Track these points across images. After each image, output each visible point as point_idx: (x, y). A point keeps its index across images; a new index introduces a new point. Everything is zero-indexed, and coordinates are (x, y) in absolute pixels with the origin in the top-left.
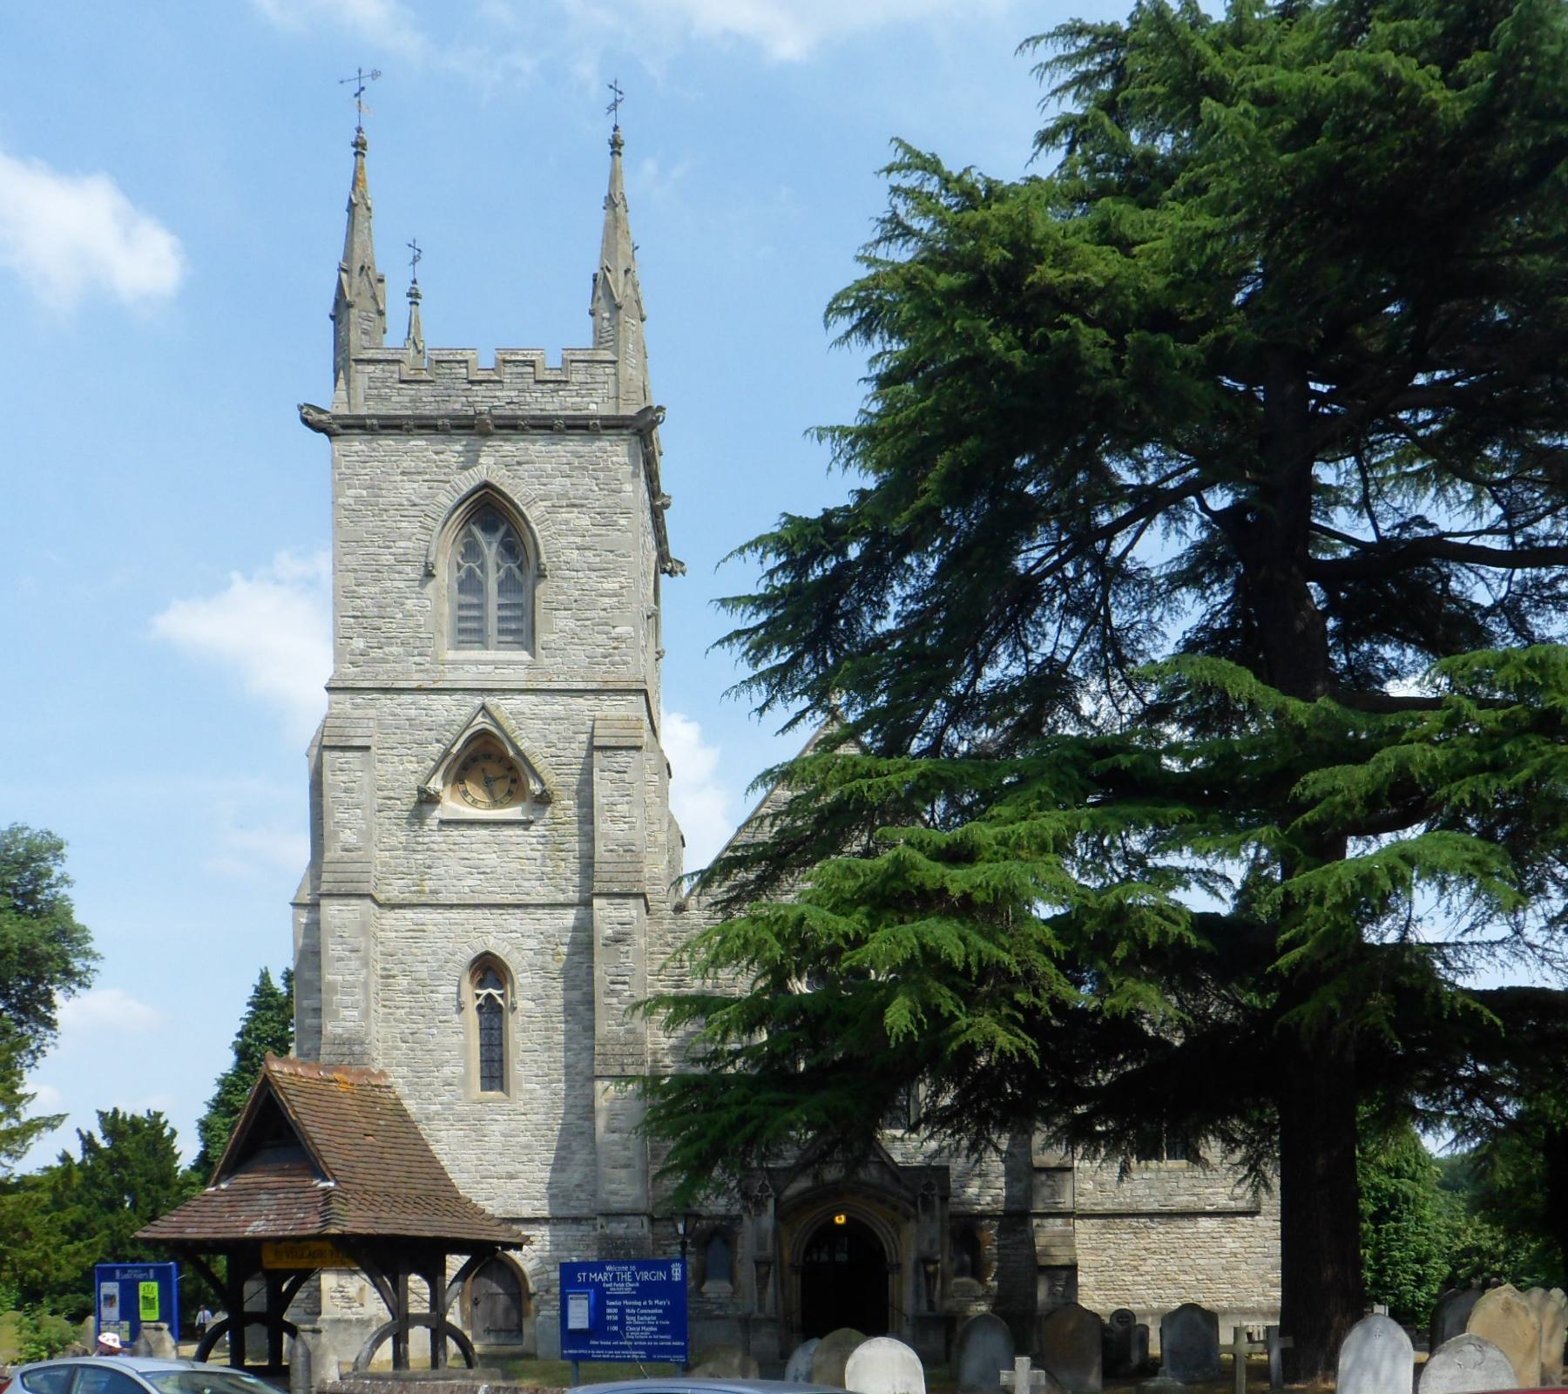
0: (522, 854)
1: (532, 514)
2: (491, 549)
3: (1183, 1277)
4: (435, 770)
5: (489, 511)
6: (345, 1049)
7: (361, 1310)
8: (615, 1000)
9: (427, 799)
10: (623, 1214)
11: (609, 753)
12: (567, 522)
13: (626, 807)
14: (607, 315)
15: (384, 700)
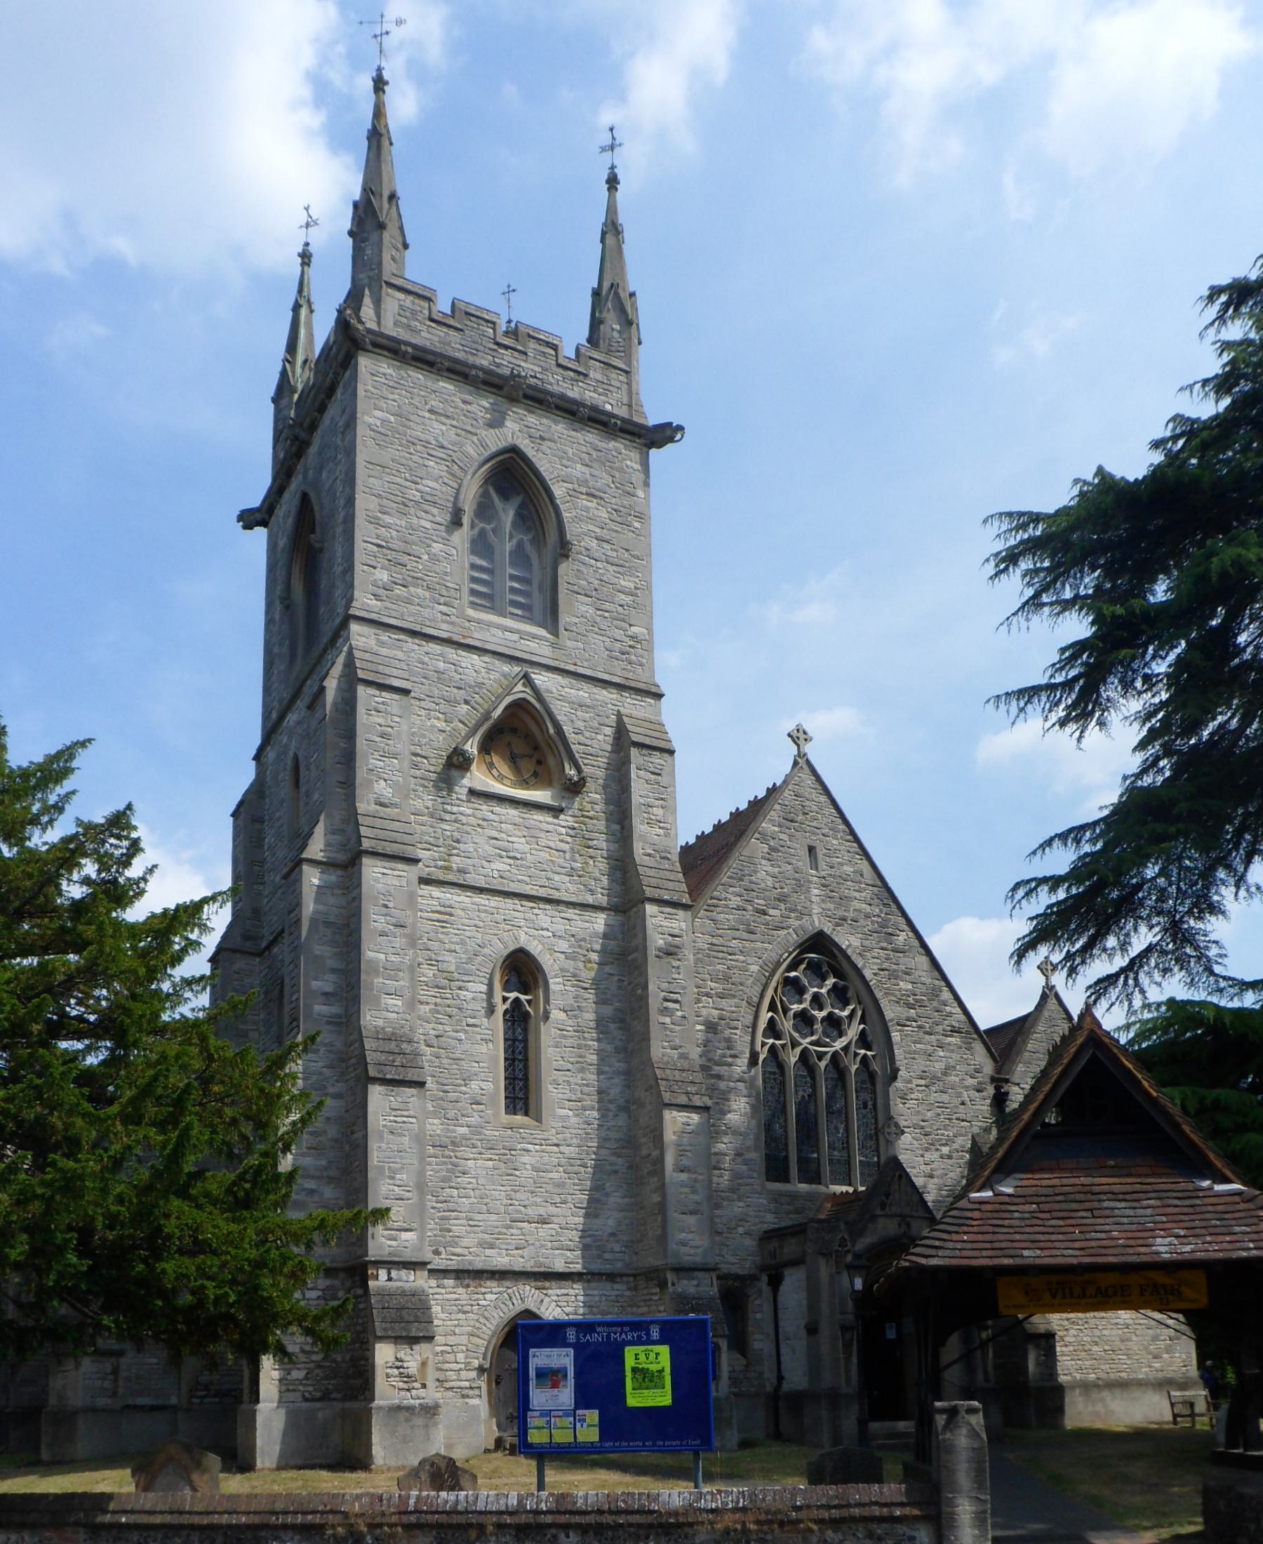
0: (552, 844)
1: (558, 491)
2: (507, 514)
3: (1095, 1348)
5: (512, 476)
6: (392, 1046)
7: (422, 1392)
8: (668, 1020)
9: (457, 762)
10: (694, 1270)
11: (644, 752)
12: (587, 509)
14: (618, 327)
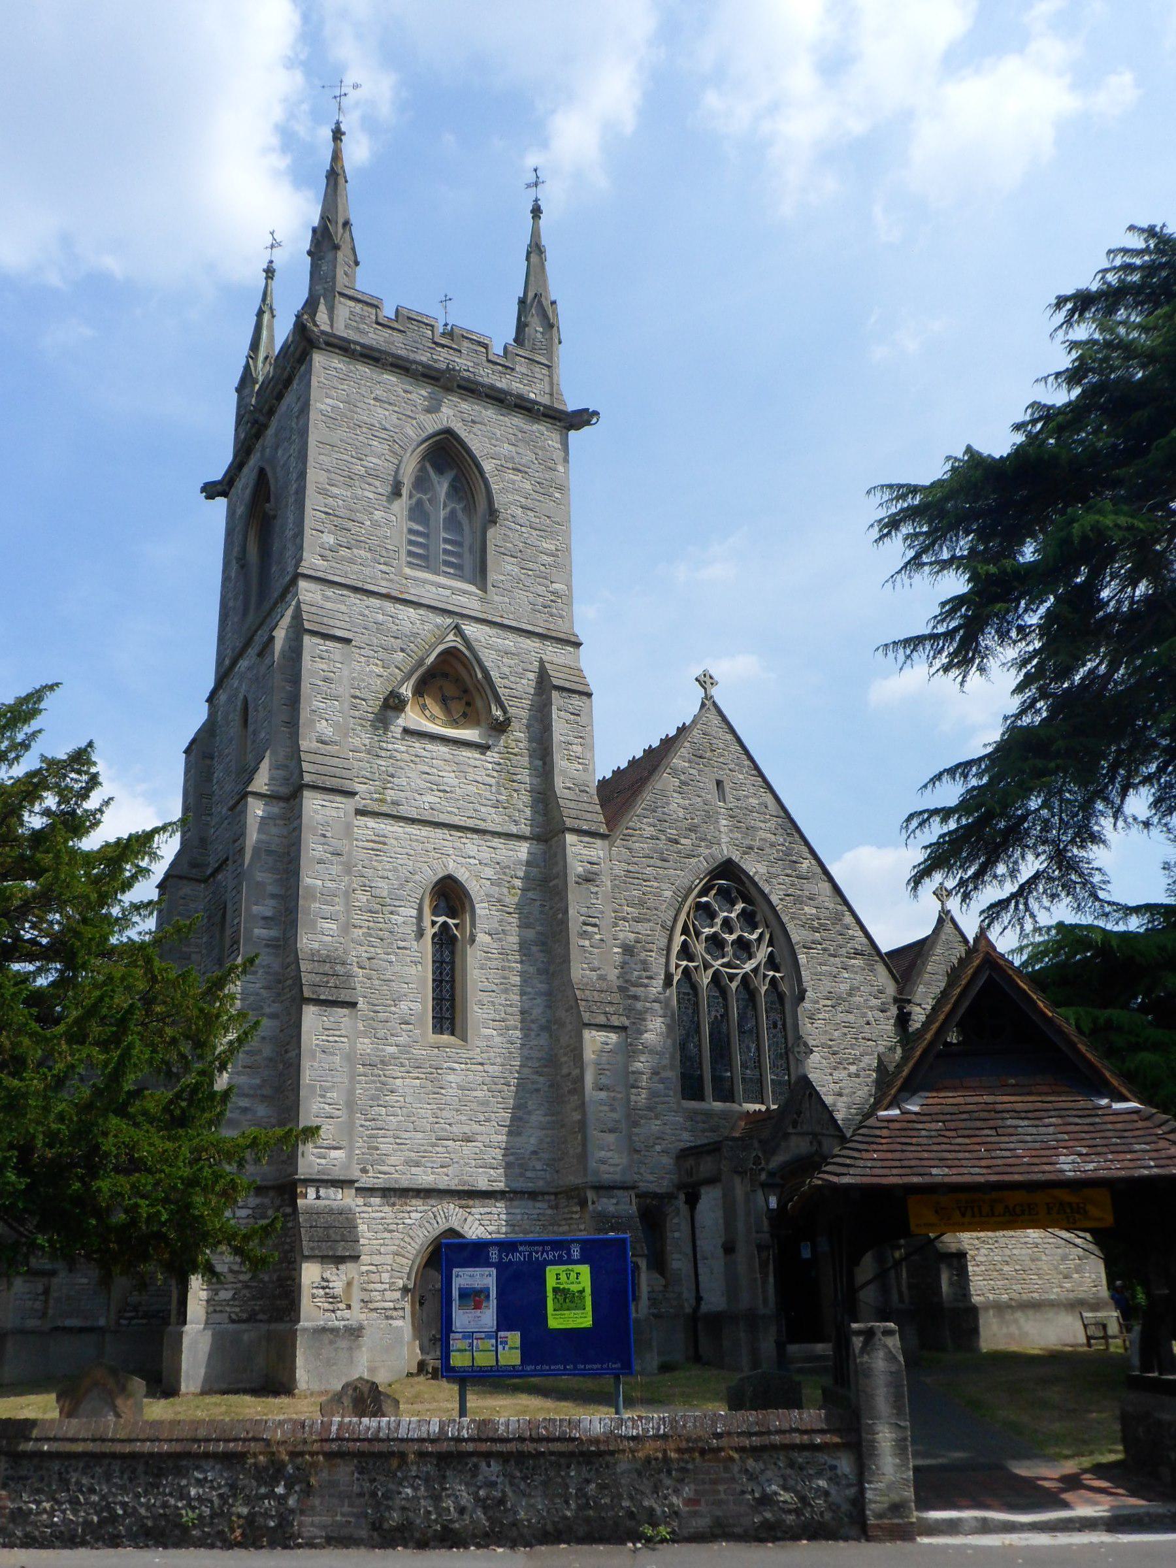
0: (479, 779)
1: (488, 466)
2: (442, 487)
3: (1006, 1268)
4: (407, 677)
5: (447, 454)
6: (327, 968)
7: (346, 1314)
8: (587, 943)
9: (393, 704)
13: (579, 749)
15: (354, 599)
